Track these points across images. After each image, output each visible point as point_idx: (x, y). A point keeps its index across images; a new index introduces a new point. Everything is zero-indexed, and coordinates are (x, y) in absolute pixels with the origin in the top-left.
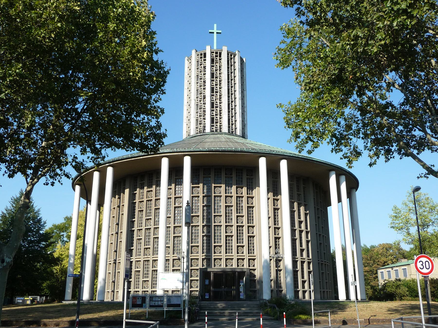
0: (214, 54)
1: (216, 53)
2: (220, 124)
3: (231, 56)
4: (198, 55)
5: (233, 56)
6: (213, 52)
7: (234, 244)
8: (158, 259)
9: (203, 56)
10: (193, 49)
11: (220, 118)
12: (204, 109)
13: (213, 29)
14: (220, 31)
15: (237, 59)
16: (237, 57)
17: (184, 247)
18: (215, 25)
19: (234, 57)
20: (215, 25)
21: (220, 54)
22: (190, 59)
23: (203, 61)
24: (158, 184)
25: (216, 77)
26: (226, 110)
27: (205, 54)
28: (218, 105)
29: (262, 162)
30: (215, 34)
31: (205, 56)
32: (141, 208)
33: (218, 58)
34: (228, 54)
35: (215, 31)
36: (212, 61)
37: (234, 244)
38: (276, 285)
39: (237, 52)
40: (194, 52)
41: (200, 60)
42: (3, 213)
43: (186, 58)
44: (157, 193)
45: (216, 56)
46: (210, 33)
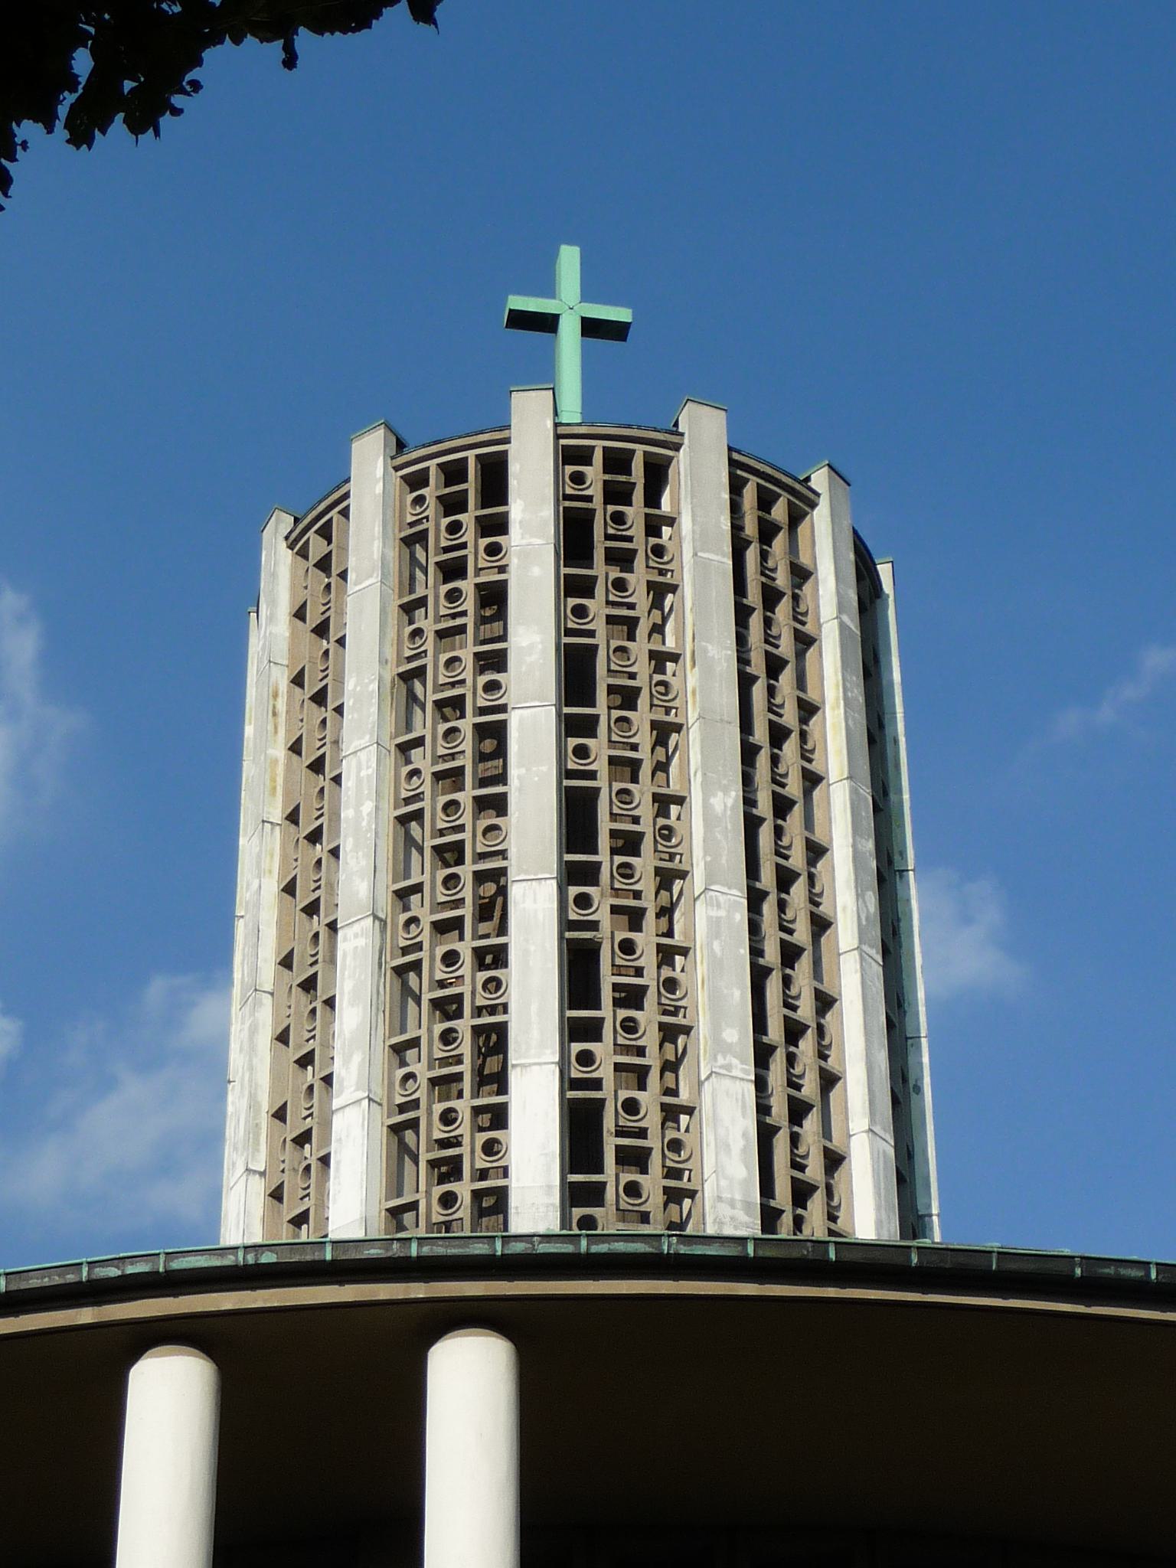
0: (595, 473)
1: (617, 462)
2: (674, 1173)
3: (765, 502)
4: (416, 481)
5: (779, 512)
9: (471, 486)
10: (361, 426)
11: (653, 527)
12: (483, 1174)
13: (550, 292)
15: (823, 541)
16: (821, 518)
17: (534, 1008)
18: (569, 260)
19: (796, 518)
20: (569, 260)
21: (657, 475)
23: (469, 535)
26: (738, 1034)
27: (495, 479)
28: (654, 1142)
30: (569, 332)
33: (635, 512)
34: (736, 487)
35: (568, 301)
36: (575, 536)
39: (820, 480)
40: (370, 466)
41: (436, 524)
42: (104, 133)
43: (280, 524)
45: (617, 494)
46: (521, 320)
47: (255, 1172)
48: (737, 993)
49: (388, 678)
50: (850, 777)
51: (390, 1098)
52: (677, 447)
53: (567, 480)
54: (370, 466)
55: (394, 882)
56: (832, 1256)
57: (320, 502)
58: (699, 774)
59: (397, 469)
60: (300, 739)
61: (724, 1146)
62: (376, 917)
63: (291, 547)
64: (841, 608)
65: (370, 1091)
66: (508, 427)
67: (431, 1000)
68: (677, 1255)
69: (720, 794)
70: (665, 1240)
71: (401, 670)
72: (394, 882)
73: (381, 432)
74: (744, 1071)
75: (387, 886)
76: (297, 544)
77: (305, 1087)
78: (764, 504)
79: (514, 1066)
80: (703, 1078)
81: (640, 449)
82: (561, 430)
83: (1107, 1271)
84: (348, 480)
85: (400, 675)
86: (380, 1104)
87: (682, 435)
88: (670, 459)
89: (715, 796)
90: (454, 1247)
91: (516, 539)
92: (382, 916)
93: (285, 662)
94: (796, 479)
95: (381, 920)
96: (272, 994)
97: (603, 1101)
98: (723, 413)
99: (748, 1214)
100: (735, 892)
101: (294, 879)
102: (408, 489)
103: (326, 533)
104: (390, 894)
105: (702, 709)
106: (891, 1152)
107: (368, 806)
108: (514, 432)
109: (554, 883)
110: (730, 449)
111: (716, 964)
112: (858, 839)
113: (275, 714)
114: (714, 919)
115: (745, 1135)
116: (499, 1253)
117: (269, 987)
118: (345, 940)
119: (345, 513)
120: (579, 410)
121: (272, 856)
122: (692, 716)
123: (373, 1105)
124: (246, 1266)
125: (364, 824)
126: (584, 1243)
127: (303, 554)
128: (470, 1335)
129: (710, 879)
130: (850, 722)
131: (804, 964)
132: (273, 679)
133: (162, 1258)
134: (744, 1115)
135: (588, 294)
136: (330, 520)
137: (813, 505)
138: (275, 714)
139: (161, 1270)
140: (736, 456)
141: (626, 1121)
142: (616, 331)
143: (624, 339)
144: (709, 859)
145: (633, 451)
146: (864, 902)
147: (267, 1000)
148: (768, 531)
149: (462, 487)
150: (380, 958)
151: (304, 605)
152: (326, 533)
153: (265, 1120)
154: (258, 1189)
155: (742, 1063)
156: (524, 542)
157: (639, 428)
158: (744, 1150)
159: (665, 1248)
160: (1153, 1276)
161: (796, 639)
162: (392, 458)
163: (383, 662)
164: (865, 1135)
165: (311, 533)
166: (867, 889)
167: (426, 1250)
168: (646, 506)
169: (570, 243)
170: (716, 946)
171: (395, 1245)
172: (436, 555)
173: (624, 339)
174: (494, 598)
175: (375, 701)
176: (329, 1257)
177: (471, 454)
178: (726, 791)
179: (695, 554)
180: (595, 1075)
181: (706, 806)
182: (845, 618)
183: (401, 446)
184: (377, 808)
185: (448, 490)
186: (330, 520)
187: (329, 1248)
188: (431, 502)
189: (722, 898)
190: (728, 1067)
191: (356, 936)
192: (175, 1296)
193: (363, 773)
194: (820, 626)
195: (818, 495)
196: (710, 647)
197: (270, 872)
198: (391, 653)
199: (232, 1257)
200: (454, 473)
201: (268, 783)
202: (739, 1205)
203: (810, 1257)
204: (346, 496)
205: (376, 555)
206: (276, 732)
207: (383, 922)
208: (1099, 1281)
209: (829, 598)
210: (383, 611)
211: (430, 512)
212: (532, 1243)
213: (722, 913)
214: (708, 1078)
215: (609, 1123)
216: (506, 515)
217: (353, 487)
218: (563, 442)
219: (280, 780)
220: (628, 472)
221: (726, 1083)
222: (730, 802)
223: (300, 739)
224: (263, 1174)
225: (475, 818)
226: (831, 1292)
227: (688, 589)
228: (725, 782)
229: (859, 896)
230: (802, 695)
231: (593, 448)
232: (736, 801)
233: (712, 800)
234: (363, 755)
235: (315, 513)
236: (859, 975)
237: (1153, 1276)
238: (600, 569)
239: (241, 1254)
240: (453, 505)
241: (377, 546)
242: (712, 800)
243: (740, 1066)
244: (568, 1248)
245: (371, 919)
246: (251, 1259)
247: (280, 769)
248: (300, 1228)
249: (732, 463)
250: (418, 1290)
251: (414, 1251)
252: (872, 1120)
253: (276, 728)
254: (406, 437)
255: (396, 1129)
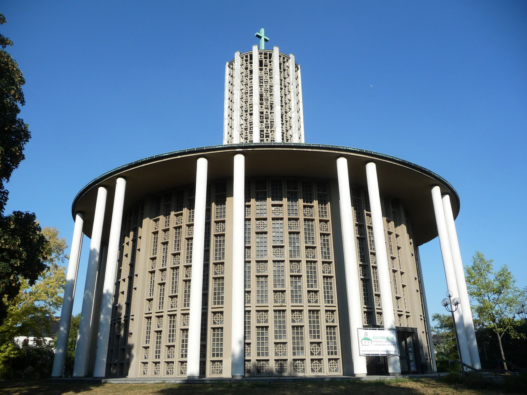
0: (263, 56)
1: (266, 54)
3: (284, 58)
4: (242, 58)
5: (285, 60)
6: (262, 54)
7: (307, 339)
8: (191, 312)
10: (236, 51)
11: (270, 62)
14: (268, 39)
20: (262, 30)
21: (270, 55)
22: (231, 63)
24: (191, 206)
25: (266, 66)
27: (251, 56)
29: (342, 165)
31: (251, 58)
32: (156, 229)
33: (268, 60)
37: (307, 339)
38: (200, 370)
40: (237, 56)
43: (227, 64)
44: (192, 217)
54: (237, 56)
76: (229, 66)
174: (251, 72)
200: (247, 57)
208: (409, 165)
226: (144, 165)
238: (264, 68)
240: (246, 61)
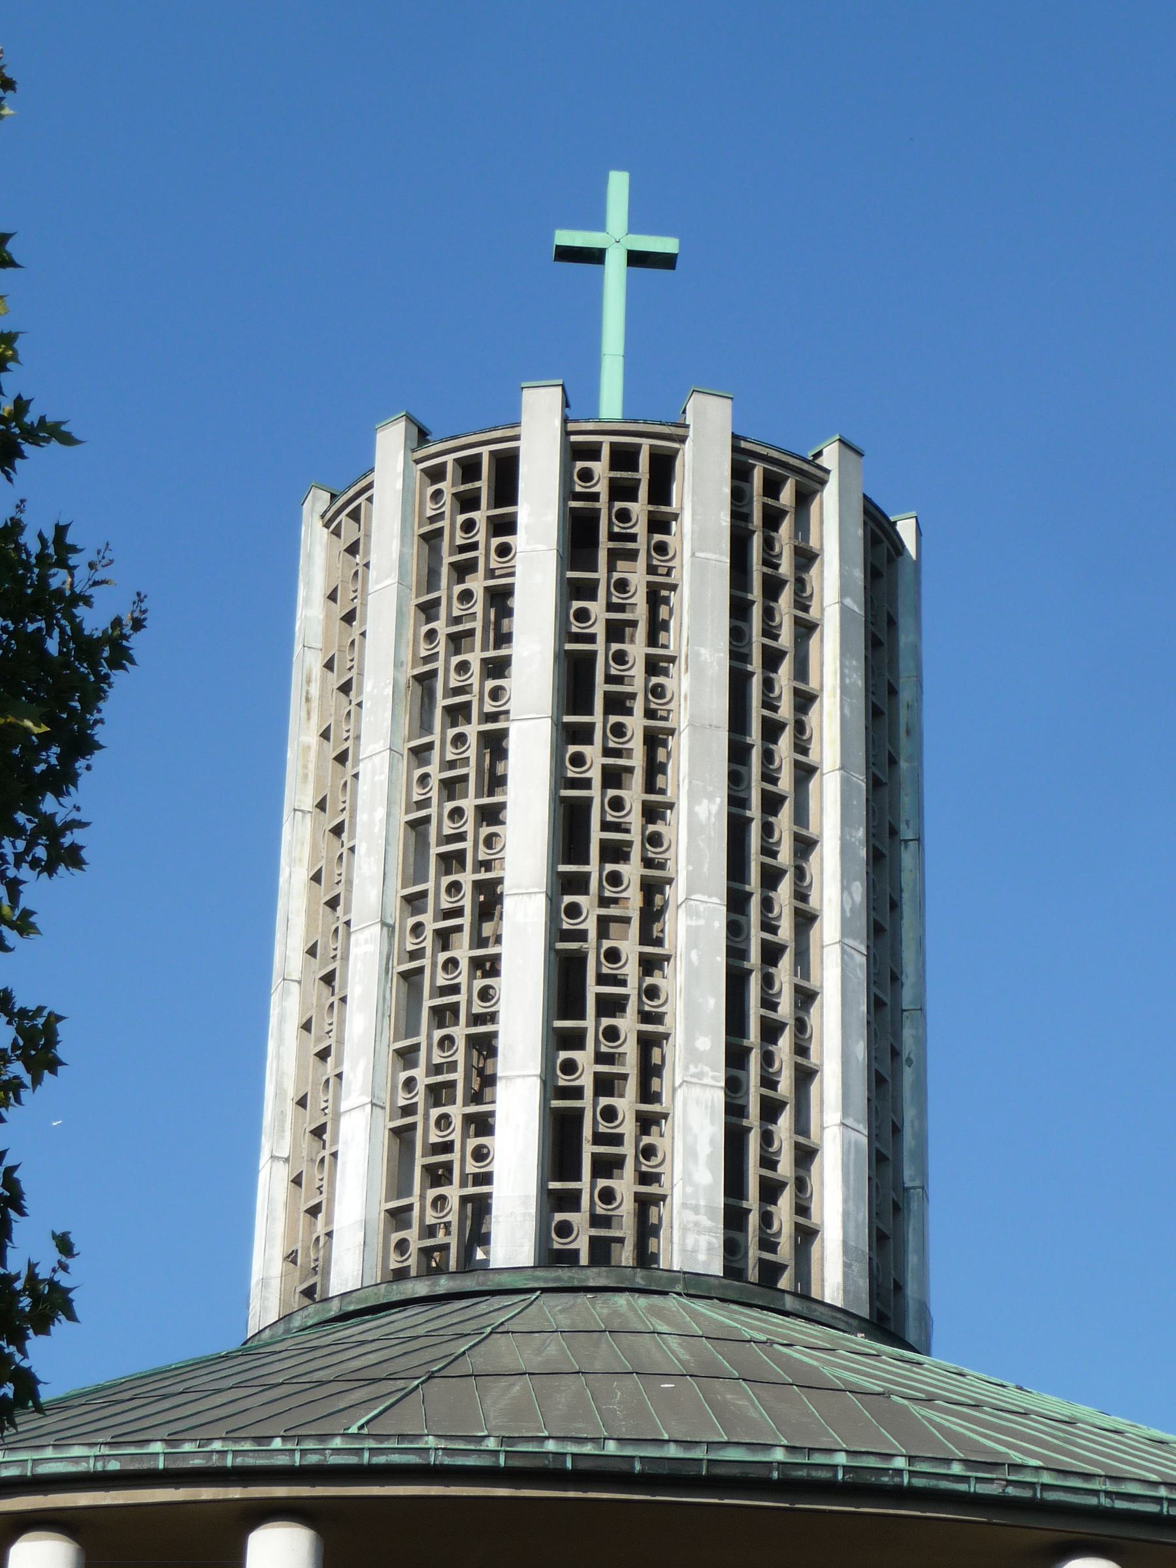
0: (601, 468)
1: (624, 458)
2: (645, 1178)
3: (772, 487)
4: (435, 475)
5: (787, 496)
9: (483, 485)
10: (383, 415)
15: (831, 524)
16: (829, 500)
18: (618, 184)
19: (804, 498)
20: (618, 184)
26: (711, 1041)
34: (740, 473)
35: (616, 236)
36: (578, 536)
39: (831, 457)
41: (451, 523)
43: (317, 502)
45: (622, 491)
46: (567, 254)
47: (279, 1158)
48: (712, 1002)
49: (403, 681)
50: (842, 768)
51: (393, 1100)
52: (682, 440)
53: (575, 478)
55: (403, 887)
56: (569, 1465)
57: (350, 487)
58: (686, 781)
59: (417, 462)
60: (328, 728)
61: (691, 1153)
62: (384, 924)
63: (327, 526)
64: (844, 591)
65: (373, 1096)
66: (517, 424)
67: (430, 1008)
68: (442, 1465)
69: (705, 802)
70: (432, 1453)
71: (416, 672)
72: (403, 887)
73: (401, 426)
74: (714, 1078)
75: (397, 891)
77: (324, 1078)
78: (769, 489)
79: (501, 1078)
80: (677, 1085)
81: (646, 443)
82: (571, 427)
83: (800, 1473)
84: (372, 470)
85: (414, 677)
86: (383, 1108)
87: (687, 426)
88: (677, 451)
89: (700, 803)
90: (262, 1458)
91: (520, 541)
92: (390, 921)
93: (320, 646)
94: (805, 460)
95: (388, 926)
96: (299, 982)
97: (582, 1110)
98: (729, 401)
99: (710, 1219)
100: (715, 900)
101: (320, 870)
102: (429, 481)
103: (355, 516)
104: (399, 899)
105: (692, 716)
106: (865, 1140)
107: (381, 813)
108: (523, 430)
109: (543, 896)
110: (735, 437)
111: (693, 974)
112: (847, 829)
113: (308, 700)
114: (696, 924)
115: (712, 1142)
116: (297, 1464)
117: (296, 977)
118: (357, 945)
119: (370, 500)
120: (622, 353)
121: (303, 844)
122: (684, 723)
123: (378, 1110)
124: (95, 1472)
125: (376, 830)
126: (366, 1455)
127: (337, 533)
128: (278, 1527)
129: (690, 890)
130: (847, 711)
131: (786, 962)
132: (307, 664)
133: (30, 1464)
134: (712, 1123)
135: (636, 225)
136: (359, 506)
137: (823, 483)
138: (308, 700)
139: (29, 1474)
140: (743, 444)
141: (604, 1127)
142: (666, 261)
143: (674, 268)
144: (690, 868)
145: (639, 446)
146: (851, 894)
147: (295, 988)
148: (772, 519)
149: (477, 484)
150: (387, 964)
151: (336, 589)
152: (355, 516)
153: (290, 1106)
154: (283, 1174)
155: (713, 1070)
156: (529, 548)
157: (645, 422)
158: (711, 1156)
159: (432, 1459)
160: (840, 1477)
161: (795, 623)
162: (413, 451)
163: (398, 664)
164: (837, 1128)
165: (343, 516)
166: (854, 880)
167: (239, 1461)
168: (649, 503)
169: (620, 168)
170: (694, 955)
171: (215, 1457)
172: (451, 555)
173: (674, 268)
175: (390, 705)
176: (161, 1466)
177: (485, 450)
178: (711, 798)
179: (693, 555)
180: (576, 1083)
181: (691, 813)
182: (848, 602)
183: (423, 436)
184: (388, 815)
185: (462, 488)
186: (359, 506)
187: (161, 1458)
188: (447, 498)
189: (702, 907)
190: (700, 1075)
191: (366, 942)
192: (45, 1495)
193: (377, 778)
194: (822, 610)
195: (827, 472)
196: (703, 651)
197: (300, 860)
198: (408, 657)
199: (84, 1464)
200: (469, 469)
201: (300, 770)
202: (702, 1210)
203: (551, 1466)
204: (370, 486)
205: (395, 555)
206: (309, 719)
207: (391, 928)
209: (833, 587)
210: (400, 613)
211: (447, 509)
212: (324, 1455)
213: (702, 922)
214: (680, 1086)
215: (587, 1132)
216: (515, 515)
217: (376, 477)
218: (573, 438)
219: (312, 767)
220: (635, 468)
221: (696, 1091)
222: (714, 809)
223: (328, 728)
224: (287, 1160)
225: (477, 826)
227: (686, 589)
228: (710, 789)
229: (845, 888)
230: (802, 686)
231: (601, 443)
232: (720, 807)
233: (697, 809)
234: (376, 759)
235: (351, 493)
236: (839, 969)
237: (840, 1477)
239: (92, 1461)
240: (468, 502)
241: (396, 544)
242: (697, 809)
243: (711, 1074)
244: (352, 1460)
245: (379, 926)
246: (99, 1467)
247: (313, 755)
248: (316, 1217)
249: (735, 449)
250: (235, 1493)
251: (229, 1462)
252: (845, 1112)
253: (309, 713)
254: (428, 424)
255: (396, 1132)
